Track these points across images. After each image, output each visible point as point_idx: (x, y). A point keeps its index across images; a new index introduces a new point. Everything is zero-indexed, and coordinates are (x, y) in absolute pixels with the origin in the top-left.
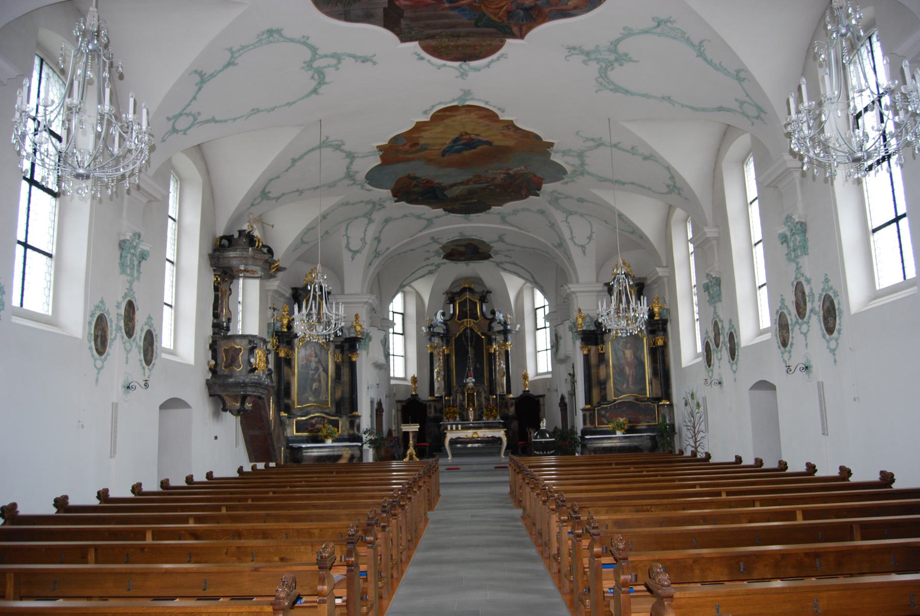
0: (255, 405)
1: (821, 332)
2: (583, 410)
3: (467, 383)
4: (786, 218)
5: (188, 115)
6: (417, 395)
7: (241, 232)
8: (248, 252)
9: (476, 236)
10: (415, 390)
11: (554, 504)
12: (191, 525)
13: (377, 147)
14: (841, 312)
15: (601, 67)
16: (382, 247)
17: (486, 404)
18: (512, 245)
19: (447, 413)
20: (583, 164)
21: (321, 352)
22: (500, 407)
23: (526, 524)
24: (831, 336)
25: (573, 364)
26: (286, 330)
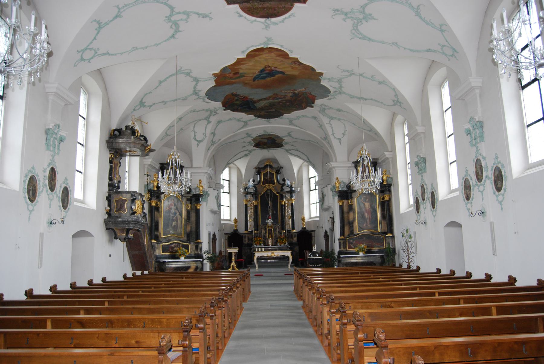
0: (135, 235)
1: (463, 199)
2: (339, 239)
3: (268, 223)
4: (470, 119)
5: (91, 49)
6: (237, 230)
7: (127, 127)
8: (131, 139)
9: (274, 133)
10: (236, 227)
11: (325, 300)
12: (82, 316)
13: (213, 74)
14: (506, 177)
15: (354, 23)
16: (216, 138)
17: (279, 235)
18: (296, 139)
19: (256, 241)
20: (341, 87)
21: (178, 203)
22: (288, 238)
23: (305, 312)
24: (499, 193)
25: (333, 211)
26: (156, 189)
